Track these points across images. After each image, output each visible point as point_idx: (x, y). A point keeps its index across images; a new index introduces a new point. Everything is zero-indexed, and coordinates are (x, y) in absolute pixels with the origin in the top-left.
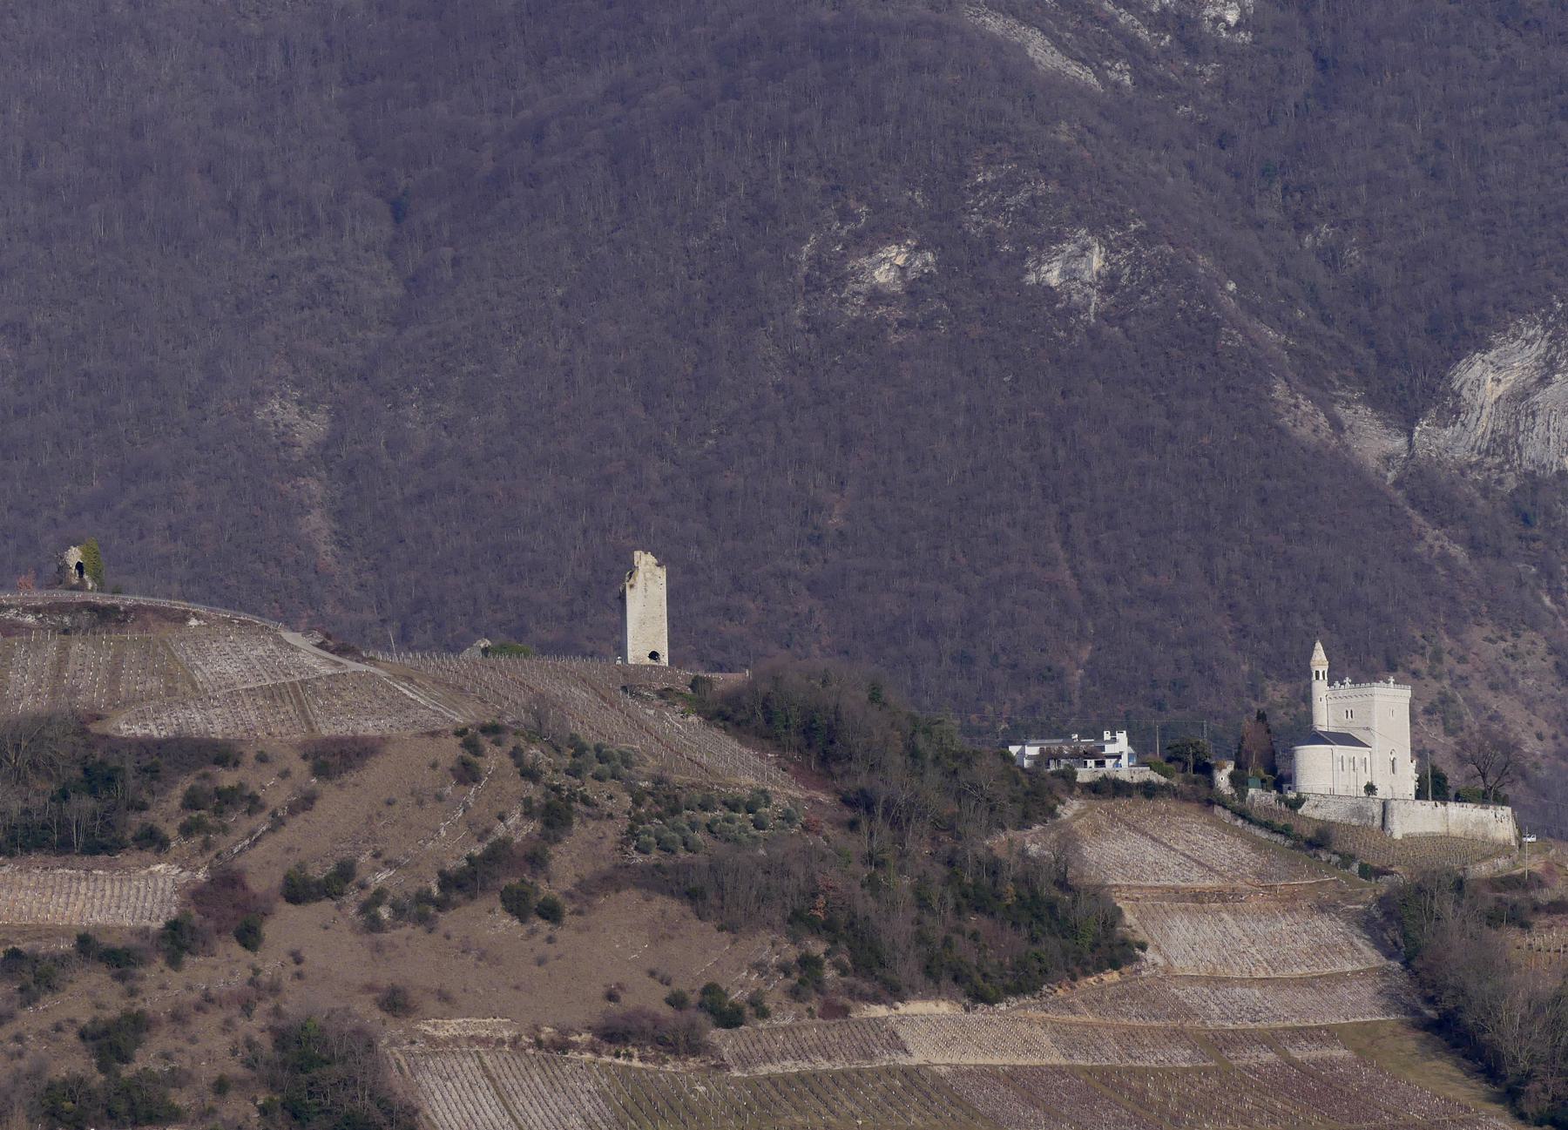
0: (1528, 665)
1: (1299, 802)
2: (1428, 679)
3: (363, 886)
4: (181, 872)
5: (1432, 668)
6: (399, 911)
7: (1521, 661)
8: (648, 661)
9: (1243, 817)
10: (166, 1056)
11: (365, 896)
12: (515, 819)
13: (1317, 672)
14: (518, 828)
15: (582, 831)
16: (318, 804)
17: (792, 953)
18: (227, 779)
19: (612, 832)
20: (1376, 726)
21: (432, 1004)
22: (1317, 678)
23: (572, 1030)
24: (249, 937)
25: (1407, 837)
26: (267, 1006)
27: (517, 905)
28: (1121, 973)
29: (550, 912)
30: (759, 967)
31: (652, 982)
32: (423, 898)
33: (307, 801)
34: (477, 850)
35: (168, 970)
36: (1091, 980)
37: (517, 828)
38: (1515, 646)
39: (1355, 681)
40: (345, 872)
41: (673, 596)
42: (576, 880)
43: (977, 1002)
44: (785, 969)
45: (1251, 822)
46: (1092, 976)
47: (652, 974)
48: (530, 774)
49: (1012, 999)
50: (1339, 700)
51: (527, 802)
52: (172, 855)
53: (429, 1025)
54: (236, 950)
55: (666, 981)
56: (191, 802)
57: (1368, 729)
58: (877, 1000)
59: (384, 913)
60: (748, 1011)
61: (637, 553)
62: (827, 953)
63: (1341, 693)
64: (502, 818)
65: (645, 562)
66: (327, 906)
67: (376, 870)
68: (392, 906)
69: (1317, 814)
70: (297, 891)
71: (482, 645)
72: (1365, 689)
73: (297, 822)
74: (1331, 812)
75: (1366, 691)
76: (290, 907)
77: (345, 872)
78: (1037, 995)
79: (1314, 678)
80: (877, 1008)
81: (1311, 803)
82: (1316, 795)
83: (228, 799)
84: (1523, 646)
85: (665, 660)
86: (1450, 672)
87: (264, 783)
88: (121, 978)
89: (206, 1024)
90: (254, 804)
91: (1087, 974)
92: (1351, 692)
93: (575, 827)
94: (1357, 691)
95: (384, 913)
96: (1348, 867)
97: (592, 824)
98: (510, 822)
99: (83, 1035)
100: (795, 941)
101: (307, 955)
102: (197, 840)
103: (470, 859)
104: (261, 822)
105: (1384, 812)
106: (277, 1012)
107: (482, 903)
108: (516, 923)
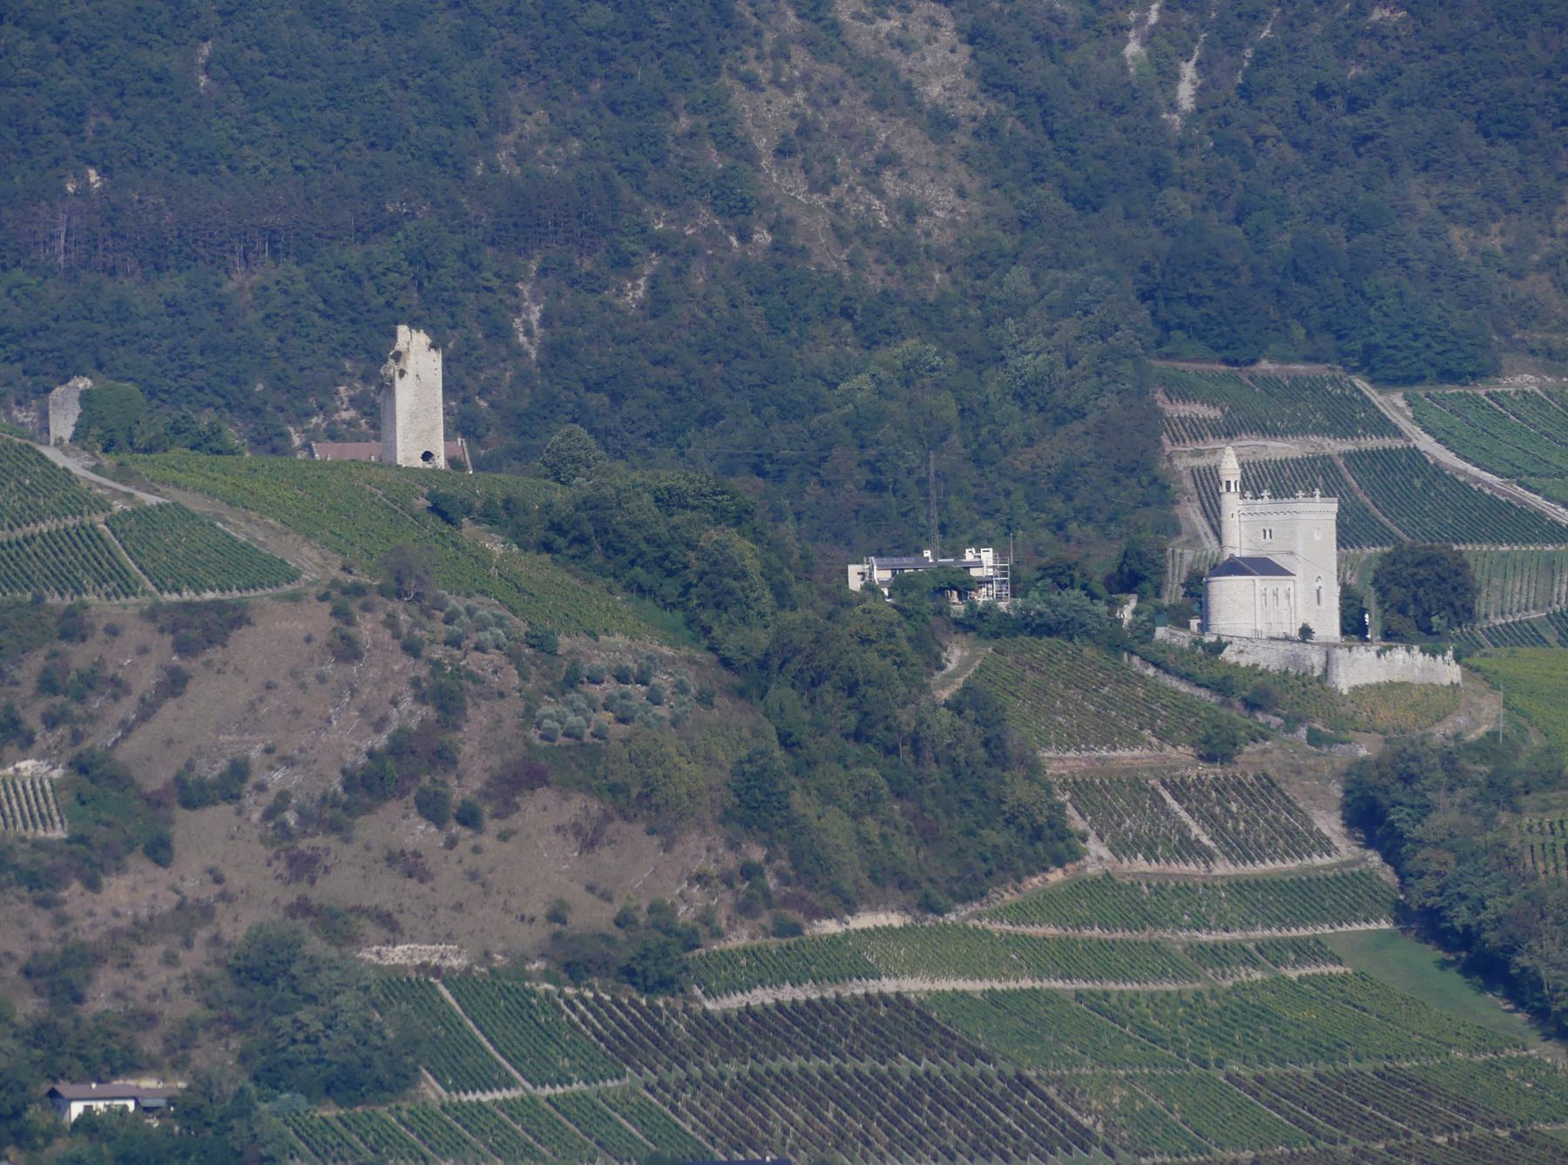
0: (929, 61)
1: (1219, 647)
2: (771, 91)
3: (261, 788)
4: (51, 770)
5: (777, 72)
6: (304, 817)
7: (917, 55)
8: (420, 463)
9: (1156, 665)
10: (119, 995)
11: (268, 799)
12: (407, 704)
13: (1228, 483)
14: (411, 714)
15: (478, 718)
16: (191, 688)
17: (731, 861)
18: (80, 656)
19: (510, 709)
20: (1300, 550)
21: (370, 929)
22: (1228, 488)
23: (527, 959)
24: (160, 851)
25: (1355, 689)
26: (203, 934)
27: (432, 808)
28: (1065, 871)
29: (469, 818)
30: (701, 879)
31: (592, 898)
32: (327, 800)
33: (174, 683)
34: (381, 741)
35: (89, 894)
36: (1035, 880)
37: (410, 714)
38: (904, 27)
39: (1275, 495)
40: (239, 770)
41: (451, 387)
42: (487, 776)
43: (927, 913)
44: (728, 881)
45: (1167, 671)
46: (1036, 876)
47: (591, 889)
48: (412, 649)
49: (959, 907)
50: (1255, 517)
51: (415, 683)
52: (36, 748)
53: (371, 952)
54: (147, 865)
55: (607, 897)
56: (47, 685)
57: (1292, 553)
58: (829, 915)
59: (291, 818)
60: (703, 931)
61: (403, 330)
62: (768, 860)
63: (1257, 509)
64: (394, 703)
65: (413, 343)
66: (223, 812)
67: (271, 768)
68: (299, 813)
69: (1245, 661)
70: (192, 794)
71: (81, 386)
72: (1288, 505)
73: (170, 707)
74: (1270, 658)
75: (1288, 507)
76: (187, 812)
77: (239, 770)
78: (985, 901)
79: (1224, 489)
80: (825, 922)
81: (1235, 648)
82: (1241, 638)
83: (90, 682)
84: (918, 29)
85: (441, 462)
86: (806, 78)
87: (121, 661)
88: (44, 903)
89: (148, 956)
90: (119, 687)
91: (1031, 874)
92: (1271, 508)
93: (470, 712)
94: (1279, 507)
95: (291, 818)
96: (1292, 731)
97: (485, 705)
98: (402, 707)
99: (27, 972)
100: (733, 846)
101: (228, 872)
102: (62, 730)
103: (371, 754)
104: (127, 708)
105: (1327, 662)
106: (216, 940)
107: (393, 808)
108: (433, 829)
